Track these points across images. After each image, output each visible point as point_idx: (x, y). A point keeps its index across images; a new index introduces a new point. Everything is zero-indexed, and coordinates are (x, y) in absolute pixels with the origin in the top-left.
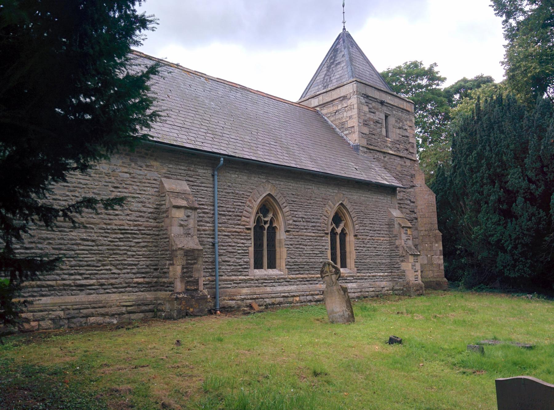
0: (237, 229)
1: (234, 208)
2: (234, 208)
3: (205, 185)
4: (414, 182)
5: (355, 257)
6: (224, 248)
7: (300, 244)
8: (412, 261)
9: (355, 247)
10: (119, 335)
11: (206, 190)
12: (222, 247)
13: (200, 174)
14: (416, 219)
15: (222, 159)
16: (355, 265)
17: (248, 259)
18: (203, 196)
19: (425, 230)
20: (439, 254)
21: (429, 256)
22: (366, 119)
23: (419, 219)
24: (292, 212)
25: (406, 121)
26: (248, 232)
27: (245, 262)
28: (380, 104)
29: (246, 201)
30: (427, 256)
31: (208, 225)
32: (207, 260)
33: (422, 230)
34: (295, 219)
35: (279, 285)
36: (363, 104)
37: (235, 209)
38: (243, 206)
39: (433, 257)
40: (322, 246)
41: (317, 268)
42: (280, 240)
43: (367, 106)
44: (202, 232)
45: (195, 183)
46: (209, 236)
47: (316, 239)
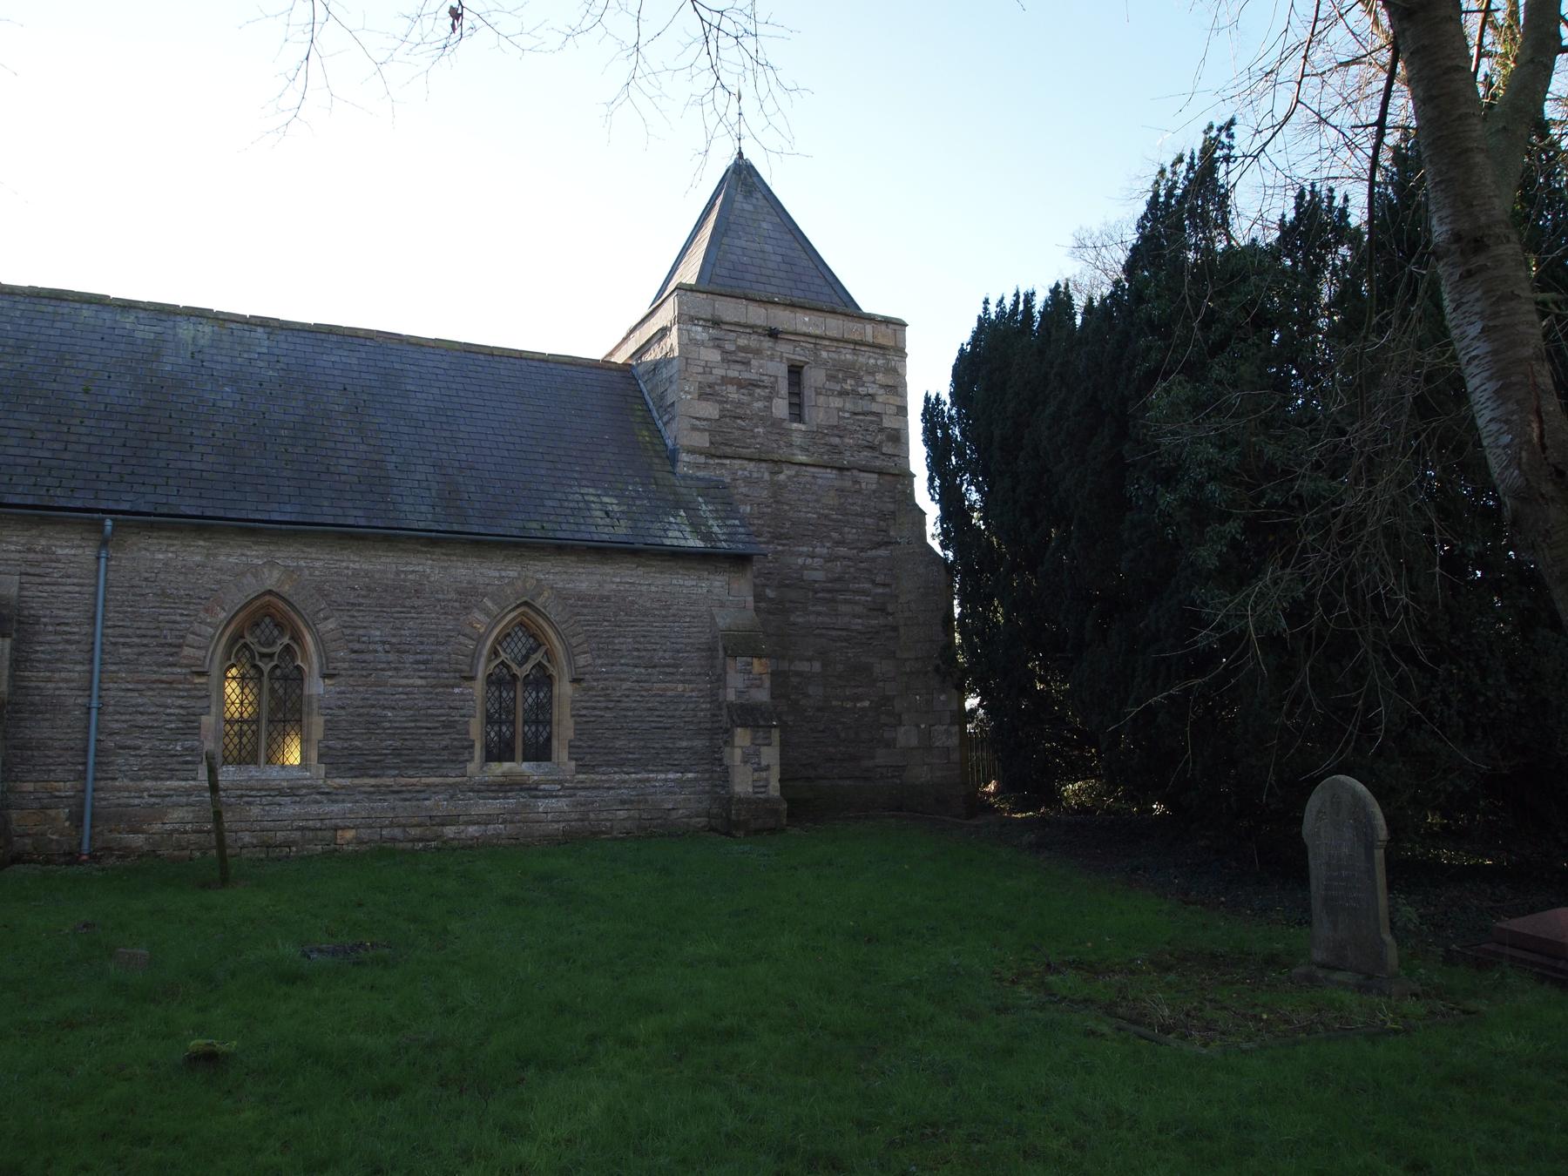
0: (166, 673)
1: (158, 628)
2: (158, 628)
3: (76, 581)
4: (892, 533)
5: (570, 734)
6: (123, 718)
7: (373, 706)
8: (747, 743)
9: (572, 709)
10: (1272, 961)
11: (79, 593)
12: (116, 717)
13: (60, 557)
14: (895, 629)
15: (109, 523)
16: (570, 753)
17: (197, 743)
18: (67, 606)
19: (917, 659)
20: (949, 721)
21: (923, 726)
22: (711, 379)
23: (902, 630)
24: (348, 631)
25: (873, 374)
26: (197, 680)
27: (187, 749)
28: (768, 339)
29: (195, 610)
30: (918, 726)
31: (78, 668)
32: (73, 745)
33: (909, 659)
34: (357, 646)
35: (294, 802)
36: (703, 344)
37: (162, 631)
38: (186, 622)
39: (933, 728)
40: (450, 708)
41: (429, 762)
42: (310, 696)
43: (718, 347)
44: (61, 685)
45: (47, 579)
46: (81, 693)
47: (428, 693)
